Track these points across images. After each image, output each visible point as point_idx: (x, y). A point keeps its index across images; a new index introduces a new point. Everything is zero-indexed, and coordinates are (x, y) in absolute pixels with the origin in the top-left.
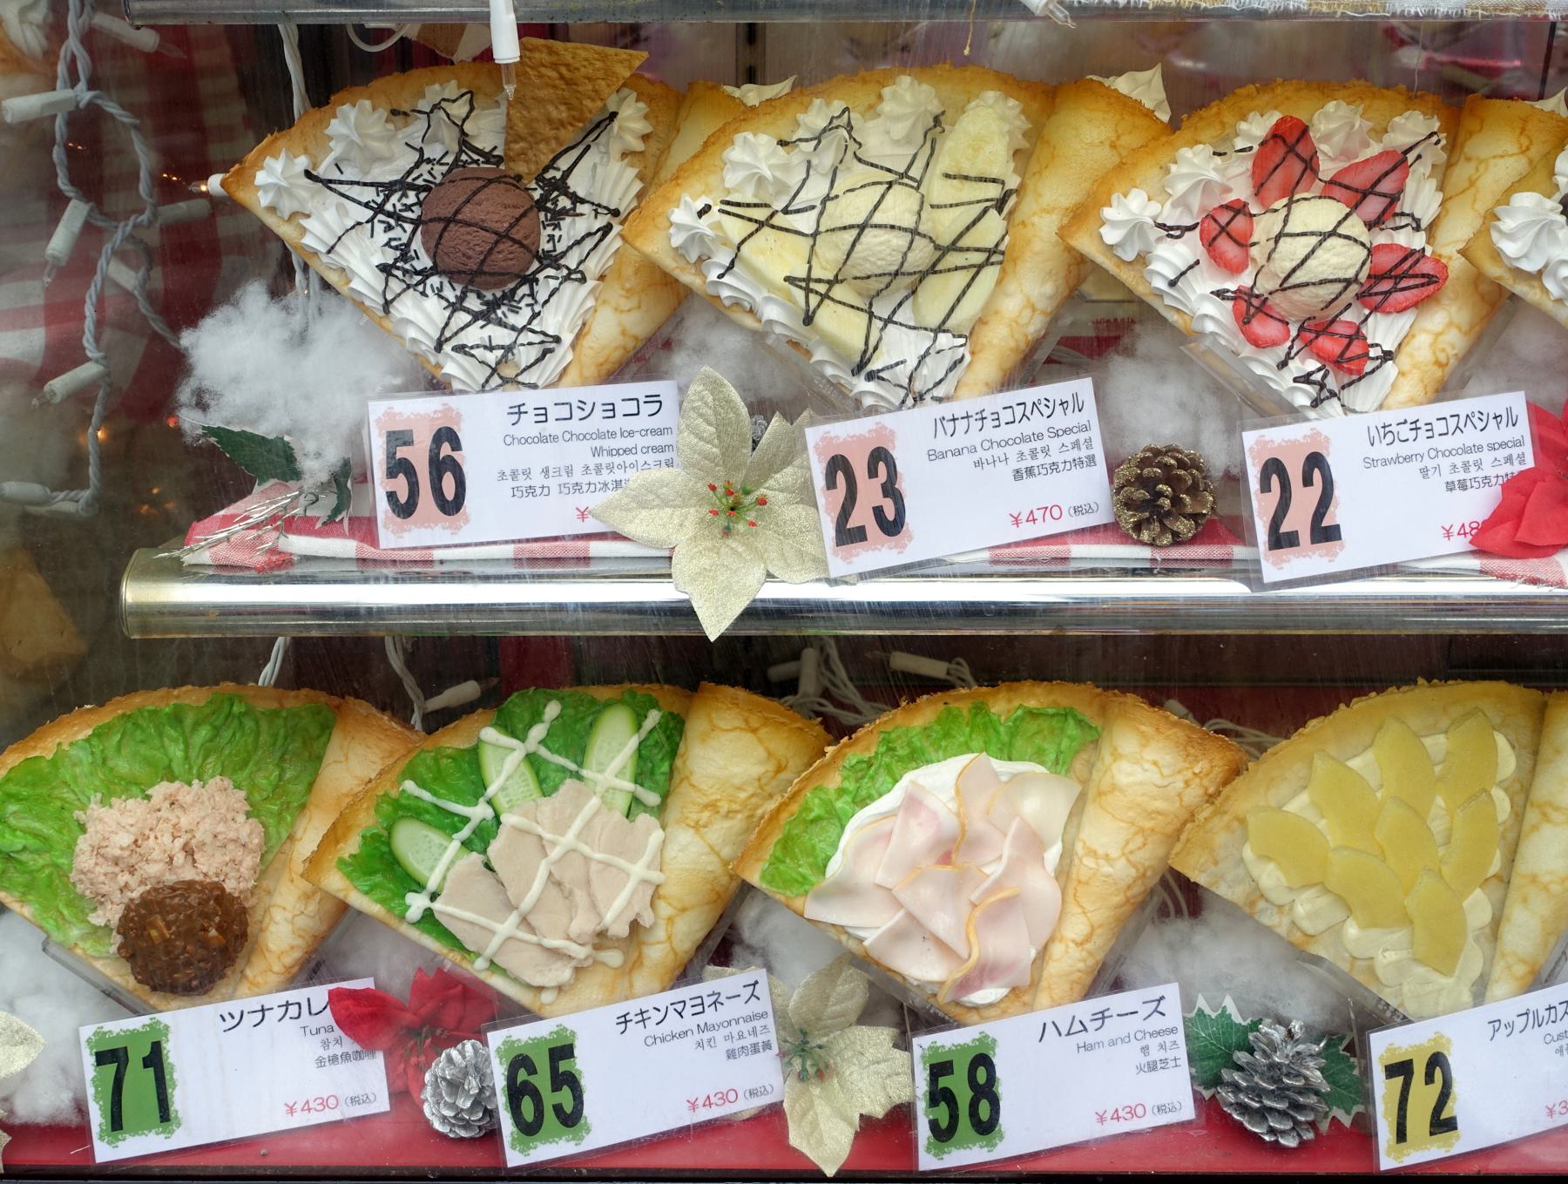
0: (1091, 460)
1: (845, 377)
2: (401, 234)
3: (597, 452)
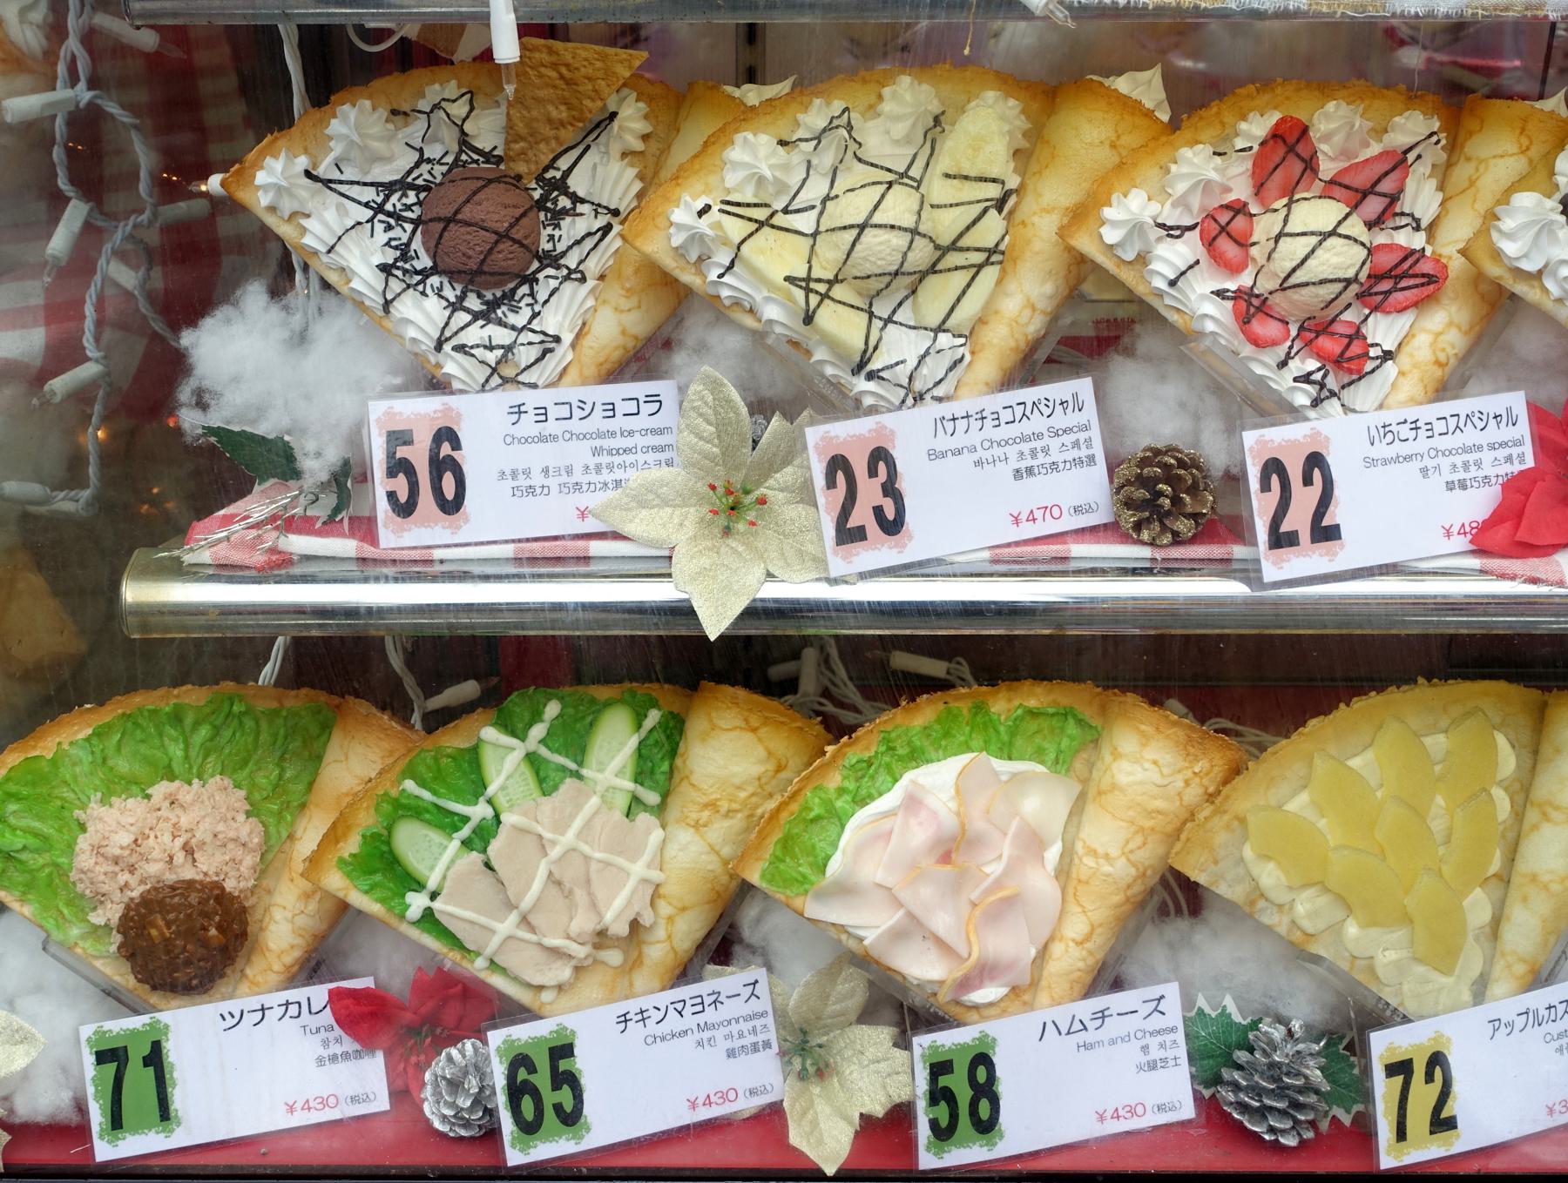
0: (1091, 459)
1: (845, 376)
2: (401, 234)
3: (597, 451)
